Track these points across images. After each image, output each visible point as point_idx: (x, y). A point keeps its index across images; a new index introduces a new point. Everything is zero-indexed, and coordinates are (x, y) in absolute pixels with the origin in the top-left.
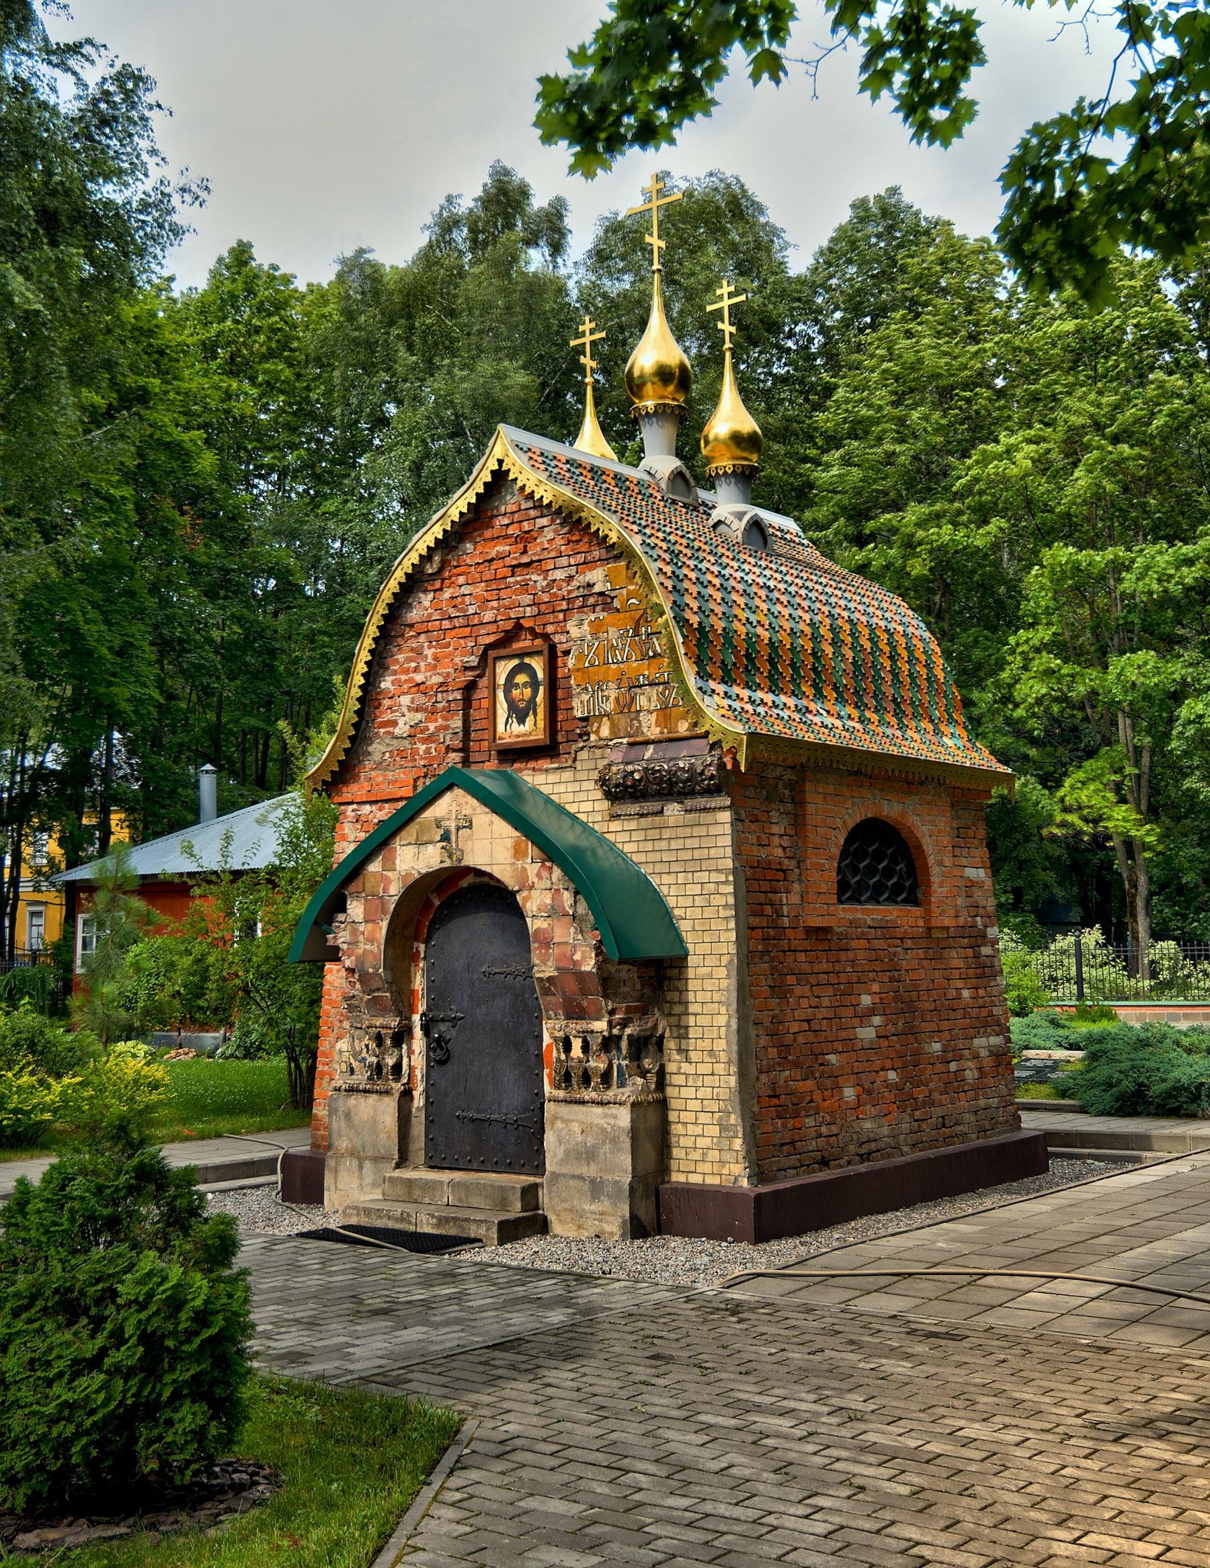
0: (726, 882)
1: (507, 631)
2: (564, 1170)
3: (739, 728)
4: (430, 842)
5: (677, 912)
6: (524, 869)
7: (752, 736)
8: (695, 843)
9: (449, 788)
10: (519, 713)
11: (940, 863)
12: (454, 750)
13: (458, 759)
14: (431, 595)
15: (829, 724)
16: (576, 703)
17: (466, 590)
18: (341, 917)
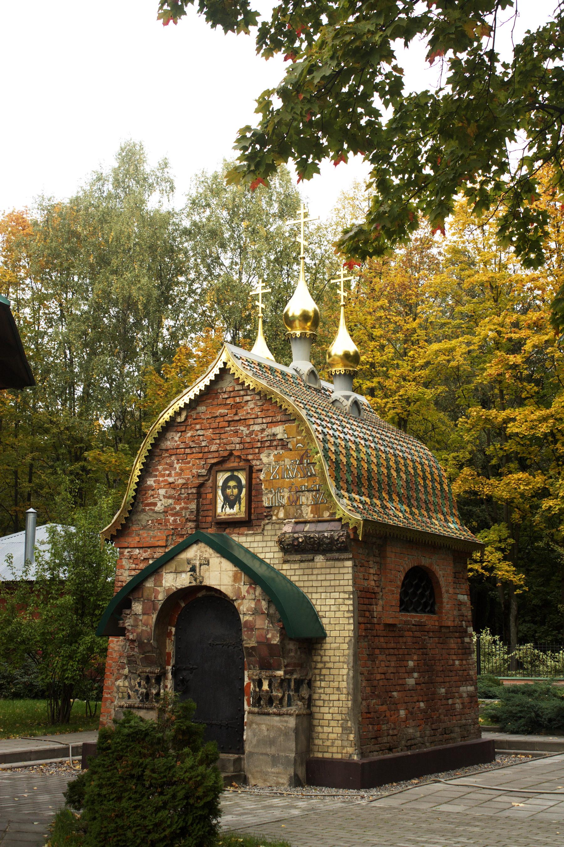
0: (349, 599)
1: (224, 457)
2: (256, 750)
3: (359, 517)
4: (184, 572)
5: (320, 614)
6: (239, 588)
7: (366, 521)
8: (332, 577)
9: (196, 542)
10: (230, 502)
11: (447, 592)
12: (190, 521)
13: (193, 526)
14: (179, 434)
15: (397, 514)
16: (264, 498)
17: (200, 432)
18: (128, 611)
